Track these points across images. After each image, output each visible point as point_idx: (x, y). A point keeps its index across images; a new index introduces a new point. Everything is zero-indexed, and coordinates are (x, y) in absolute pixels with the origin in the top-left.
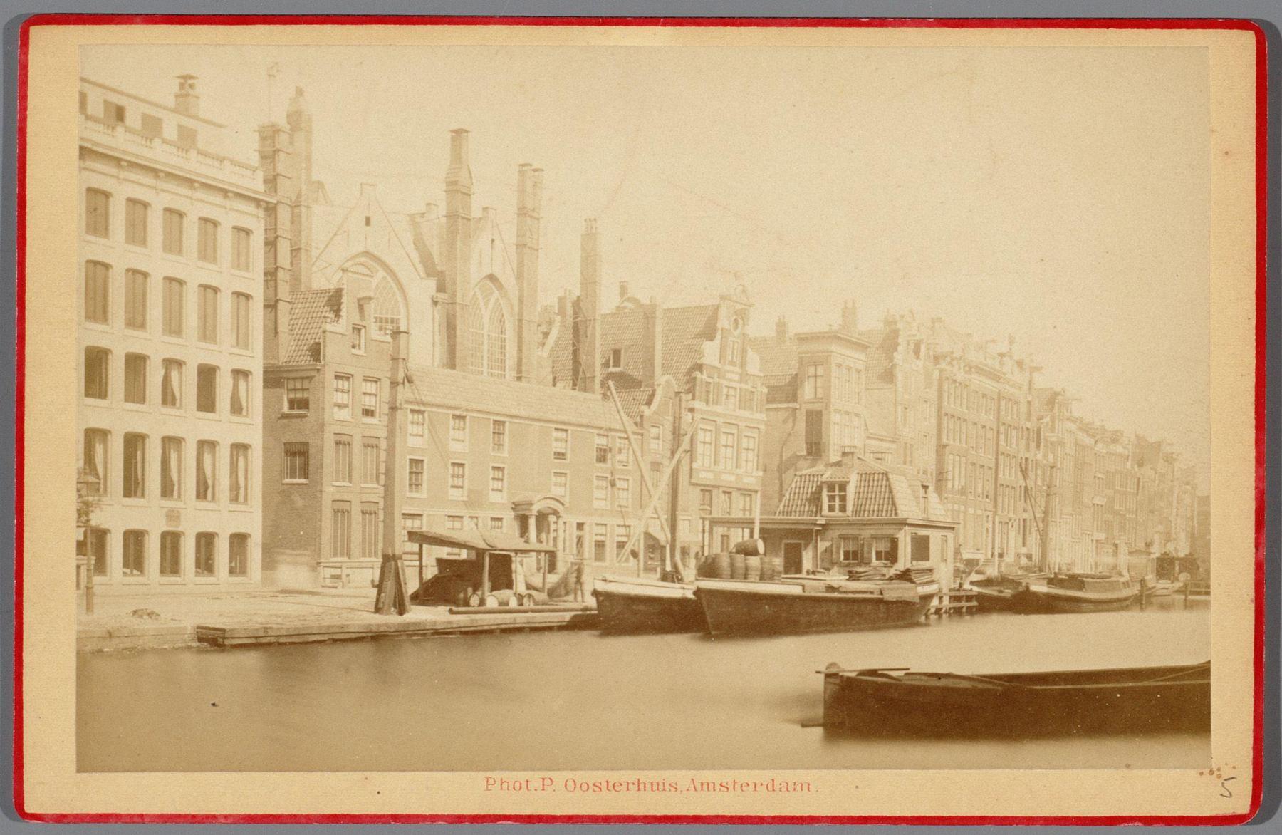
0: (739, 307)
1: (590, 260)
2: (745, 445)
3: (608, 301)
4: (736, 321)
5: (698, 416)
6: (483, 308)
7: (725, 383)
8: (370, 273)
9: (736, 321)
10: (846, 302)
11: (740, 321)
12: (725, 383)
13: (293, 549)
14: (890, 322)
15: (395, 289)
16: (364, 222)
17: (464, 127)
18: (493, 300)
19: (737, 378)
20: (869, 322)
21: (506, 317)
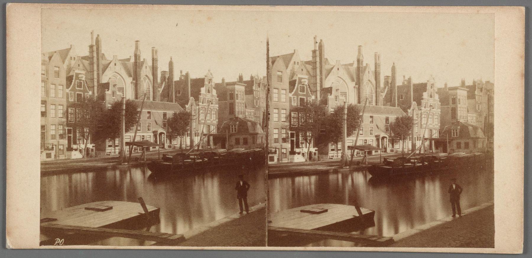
0: (210, 78)
1: (393, 69)
2: (340, 152)
3: (399, 82)
4: (209, 82)
5: (200, 107)
6: (366, 86)
7: (207, 98)
8: (115, 78)
9: (209, 82)
10: (240, 74)
11: (433, 87)
12: (207, 98)
13: (209, 153)
14: (252, 78)
15: (122, 79)
16: (337, 69)
17: (138, 40)
18: (146, 81)
19: (210, 96)
20: (247, 78)
21: (373, 90)
